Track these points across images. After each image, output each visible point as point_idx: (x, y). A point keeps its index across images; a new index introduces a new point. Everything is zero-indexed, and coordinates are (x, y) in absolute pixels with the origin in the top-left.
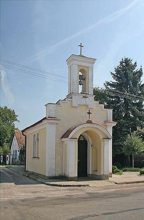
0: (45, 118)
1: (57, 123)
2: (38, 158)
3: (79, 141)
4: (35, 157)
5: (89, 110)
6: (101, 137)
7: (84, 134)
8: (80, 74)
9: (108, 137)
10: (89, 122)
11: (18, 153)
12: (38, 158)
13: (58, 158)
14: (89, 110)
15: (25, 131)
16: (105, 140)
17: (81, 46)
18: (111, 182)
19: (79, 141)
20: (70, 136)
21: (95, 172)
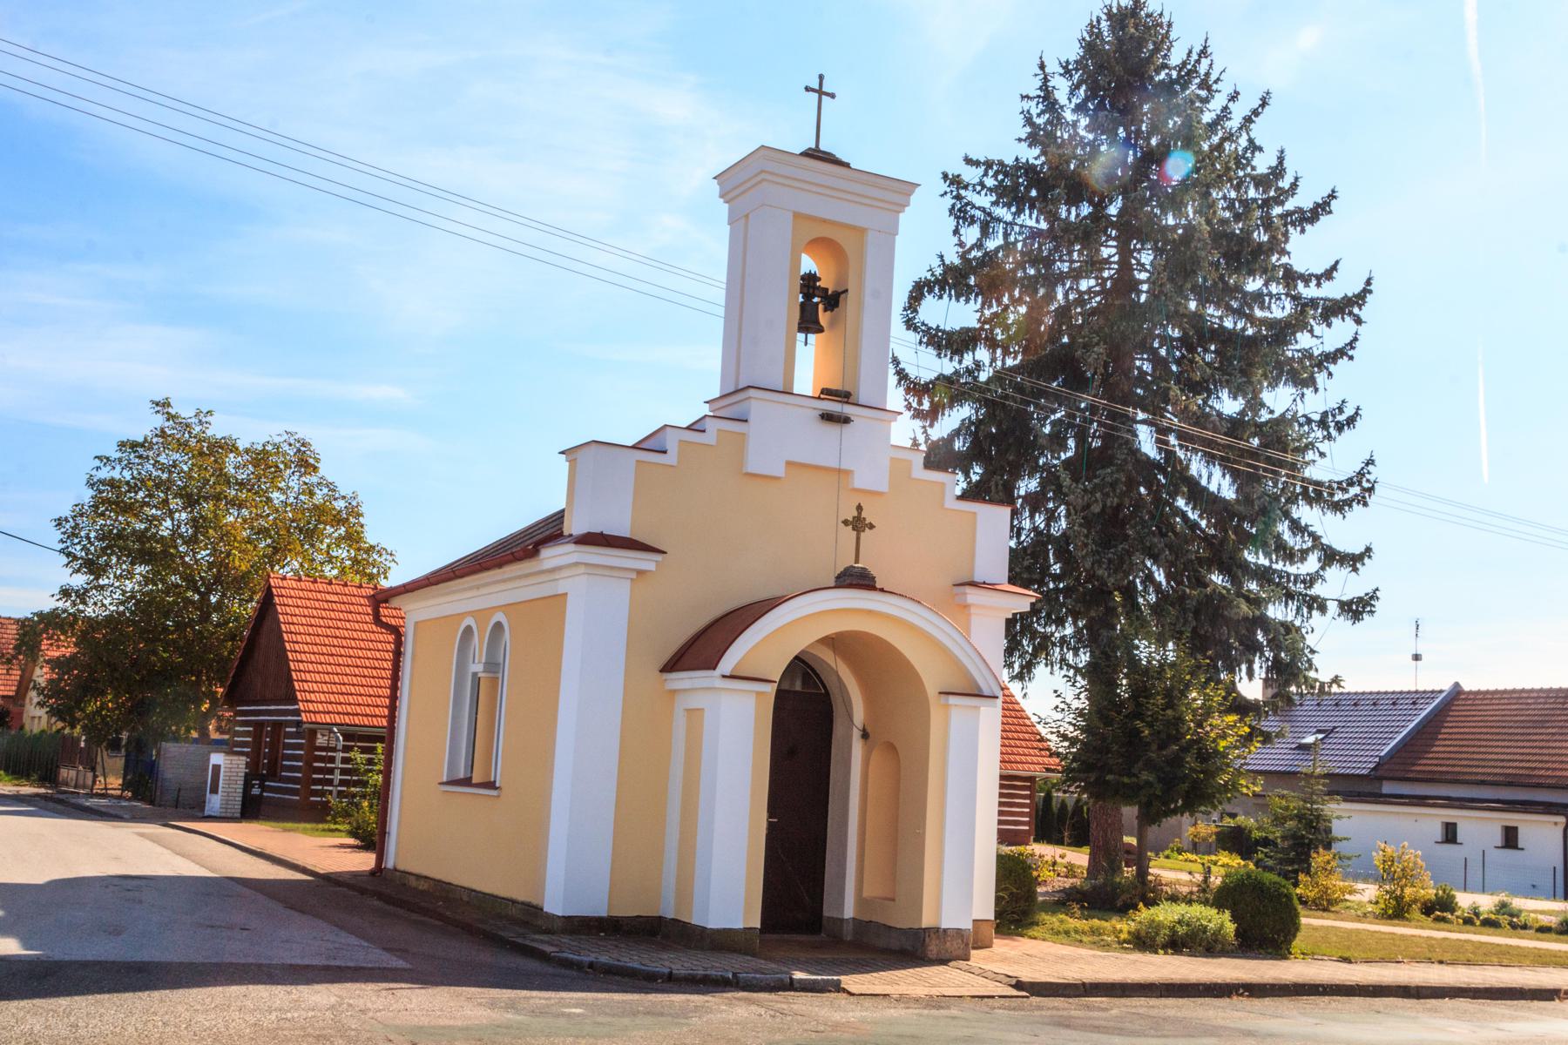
0: (548, 532)
1: (640, 573)
2: (491, 785)
3: (781, 696)
4: (467, 782)
5: (859, 508)
6: (931, 677)
7: (827, 656)
8: (808, 264)
9: (980, 689)
10: (857, 579)
11: (1104, 25)
12: (491, 785)
13: (360, 586)
14: (859, 508)
15: (395, 602)
16: (953, 700)
17: (820, 92)
18: (983, 974)
19: (784, 701)
20: (728, 663)
21: (886, 902)
